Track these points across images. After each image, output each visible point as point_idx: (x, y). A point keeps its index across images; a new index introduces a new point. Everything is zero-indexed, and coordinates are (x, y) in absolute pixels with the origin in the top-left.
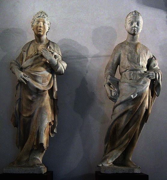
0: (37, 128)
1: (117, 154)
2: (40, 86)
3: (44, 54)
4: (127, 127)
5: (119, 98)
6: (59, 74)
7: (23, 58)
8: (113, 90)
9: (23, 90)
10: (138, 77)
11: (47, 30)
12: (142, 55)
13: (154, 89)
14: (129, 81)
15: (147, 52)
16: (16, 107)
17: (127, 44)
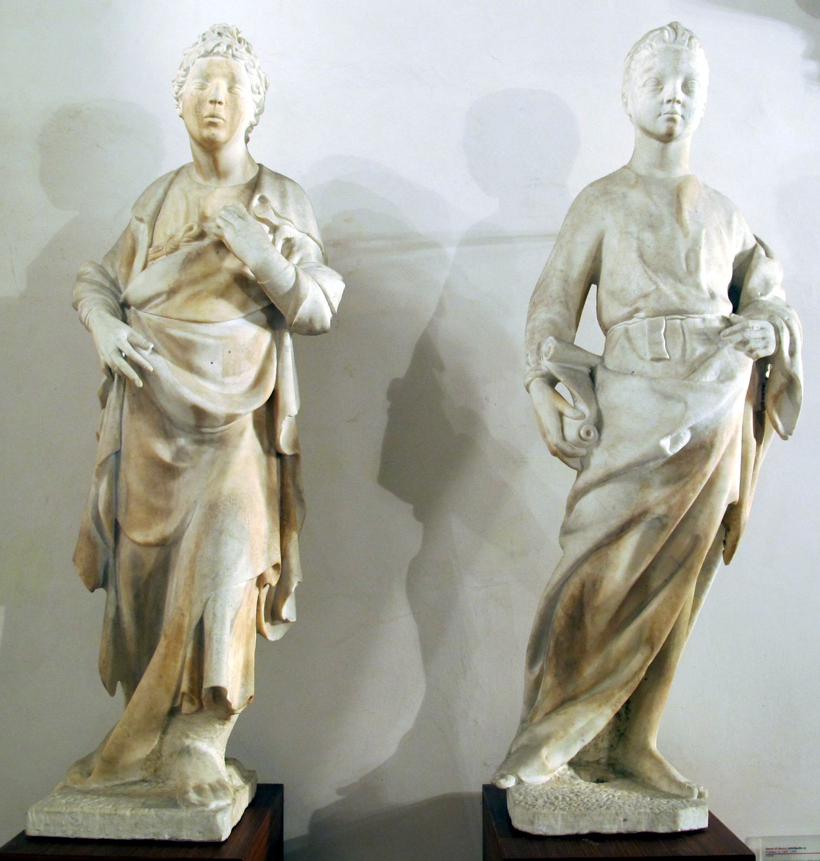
0: (196, 612)
1: (591, 721)
3: (229, 237)
4: (640, 591)
5: (599, 449)
6: (308, 331)
7: (133, 253)
8: (568, 411)
9: (132, 412)
10: (694, 350)
11: (248, 116)
12: (707, 235)
13: (769, 403)
14: (647, 367)
15: (729, 223)
16: (97, 495)
17: (633, 182)
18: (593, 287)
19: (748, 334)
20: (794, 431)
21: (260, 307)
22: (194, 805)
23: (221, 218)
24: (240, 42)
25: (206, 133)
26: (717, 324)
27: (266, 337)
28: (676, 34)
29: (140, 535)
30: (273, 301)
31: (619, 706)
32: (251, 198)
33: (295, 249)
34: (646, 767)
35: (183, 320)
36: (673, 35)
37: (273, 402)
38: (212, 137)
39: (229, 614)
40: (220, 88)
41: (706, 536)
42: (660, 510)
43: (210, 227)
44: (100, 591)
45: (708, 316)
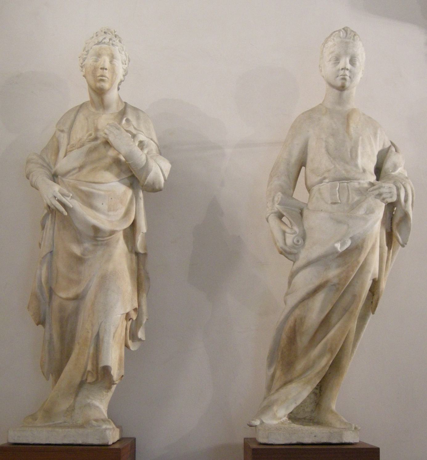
0: (96, 329)
1: (299, 393)
2: (103, 221)
3: (111, 139)
4: (325, 323)
6: (152, 189)
8: (288, 230)
11: (120, 76)
15: (375, 134)
18: (303, 168)
19: (382, 190)
20: (408, 242)
21: (118, 180)
23: (107, 129)
24: (116, 37)
25: (98, 85)
26: (366, 185)
27: (130, 193)
28: (347, 33)
29: (64, 293)
30: (134, 173)
31: (315, 386)
32: (121, 119)
33: (145, 147)
34: (330, 418)
35: (87, 182)
36: (345, 35)
37: (134, 225)
38: (102, 87)
39: (113, 330)
40: (105, 61)
41: (360, 296)
42: (335, 281)
43: (101, 134)
44: (40, 326)
45: (362, 182)
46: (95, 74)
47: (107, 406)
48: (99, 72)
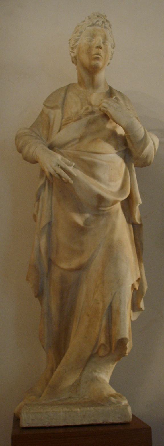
0: (108, 300)
22: (114, 403)
25: (93, 62)
46: (90, 53)
47: (109, 378)
48: (94, 51)
